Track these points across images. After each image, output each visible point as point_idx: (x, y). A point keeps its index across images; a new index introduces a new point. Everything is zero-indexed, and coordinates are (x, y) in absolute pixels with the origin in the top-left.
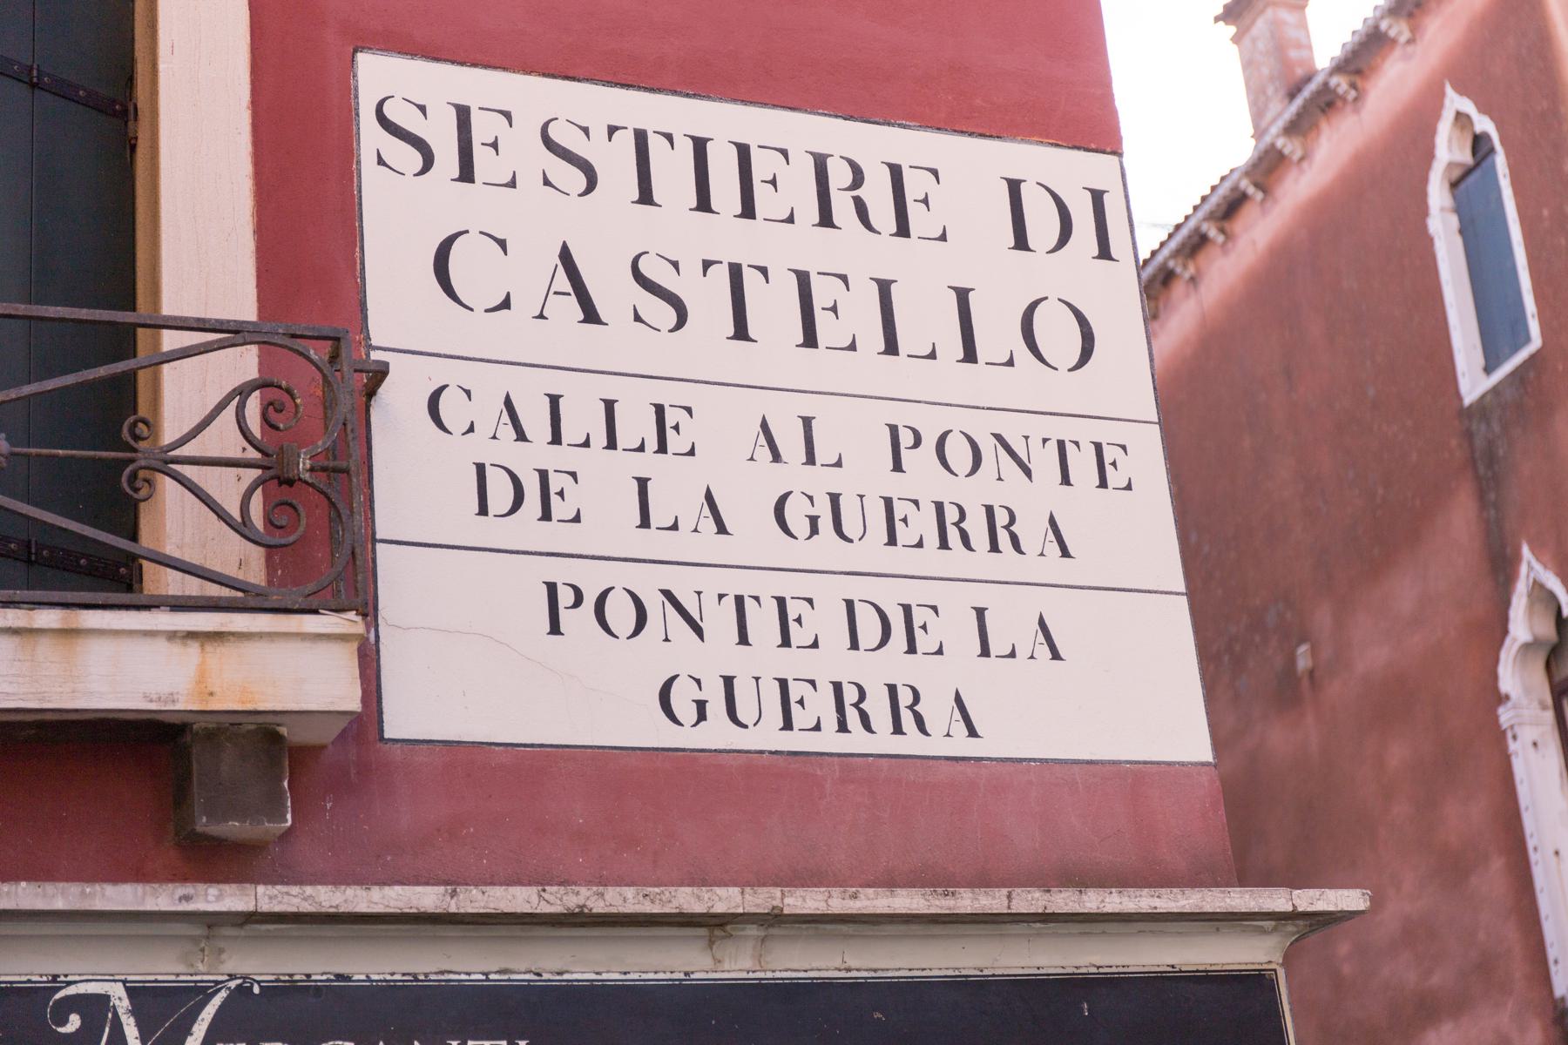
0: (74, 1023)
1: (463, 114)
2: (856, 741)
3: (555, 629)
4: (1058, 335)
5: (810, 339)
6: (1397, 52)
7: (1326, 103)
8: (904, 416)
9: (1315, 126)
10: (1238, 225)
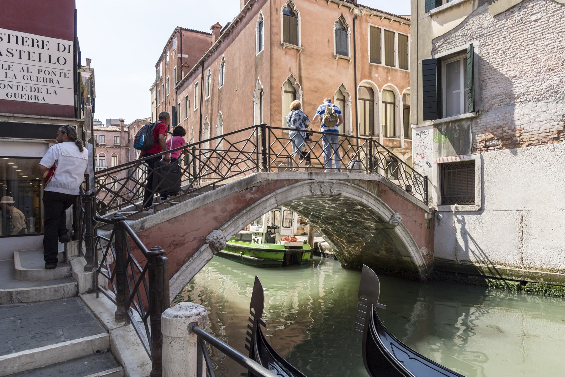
2: (30, 101)
4: (62, 61)
5: (29, 59)
8: (40, 68)
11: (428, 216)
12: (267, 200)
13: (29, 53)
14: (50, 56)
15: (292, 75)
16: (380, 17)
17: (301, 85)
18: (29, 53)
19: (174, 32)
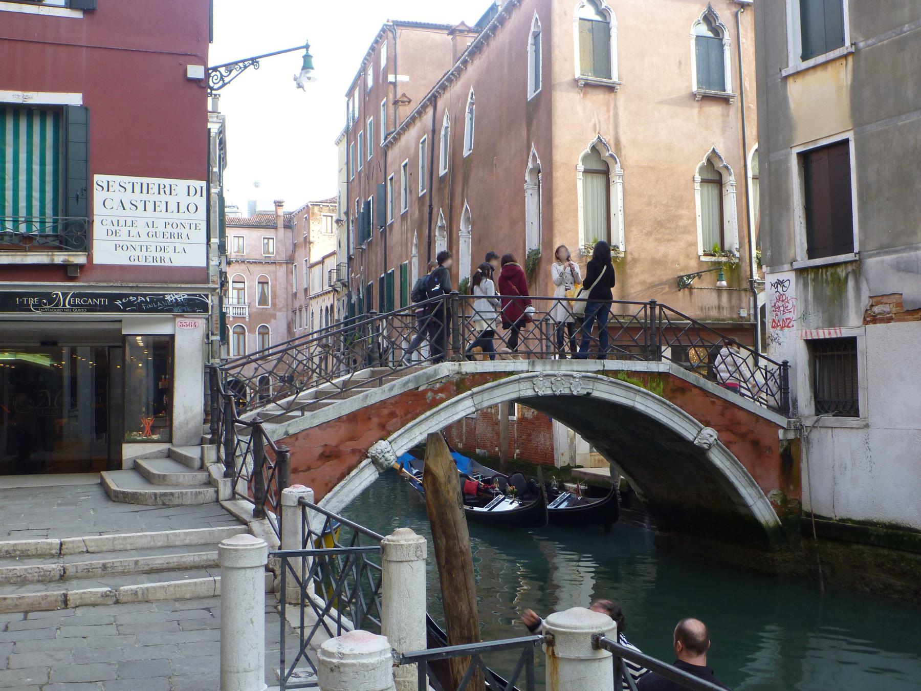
0: (55, 296)
2: (155, 264)
8: (167, 221)
11: (785, 434)
12: (457, 402)
13: (155, 202)
14: (178, 203)
15: (599, 137)
18: (155, 202)
19: (381, 30)
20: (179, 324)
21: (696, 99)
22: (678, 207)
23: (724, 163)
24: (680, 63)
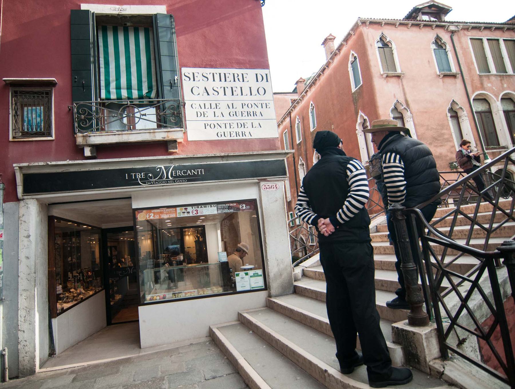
0: (159, 170)
1: (193, 74)
2: (238, 138)
3: (205, 128)
4: (261, 91)
5: (233, 95)
6: (345, 46)
7: (336, 55)
8: (243, 102)
9: (334, 58)
10: (325, 72)
13: (232, 88)
15: (397, 100)
16: (479, 28)
17: (409, 108)
18: (232, 88)
20: (263, 187)
21: (440, 77)
22: (442, 129)
23: (460, 106)
24: (429, 61)
